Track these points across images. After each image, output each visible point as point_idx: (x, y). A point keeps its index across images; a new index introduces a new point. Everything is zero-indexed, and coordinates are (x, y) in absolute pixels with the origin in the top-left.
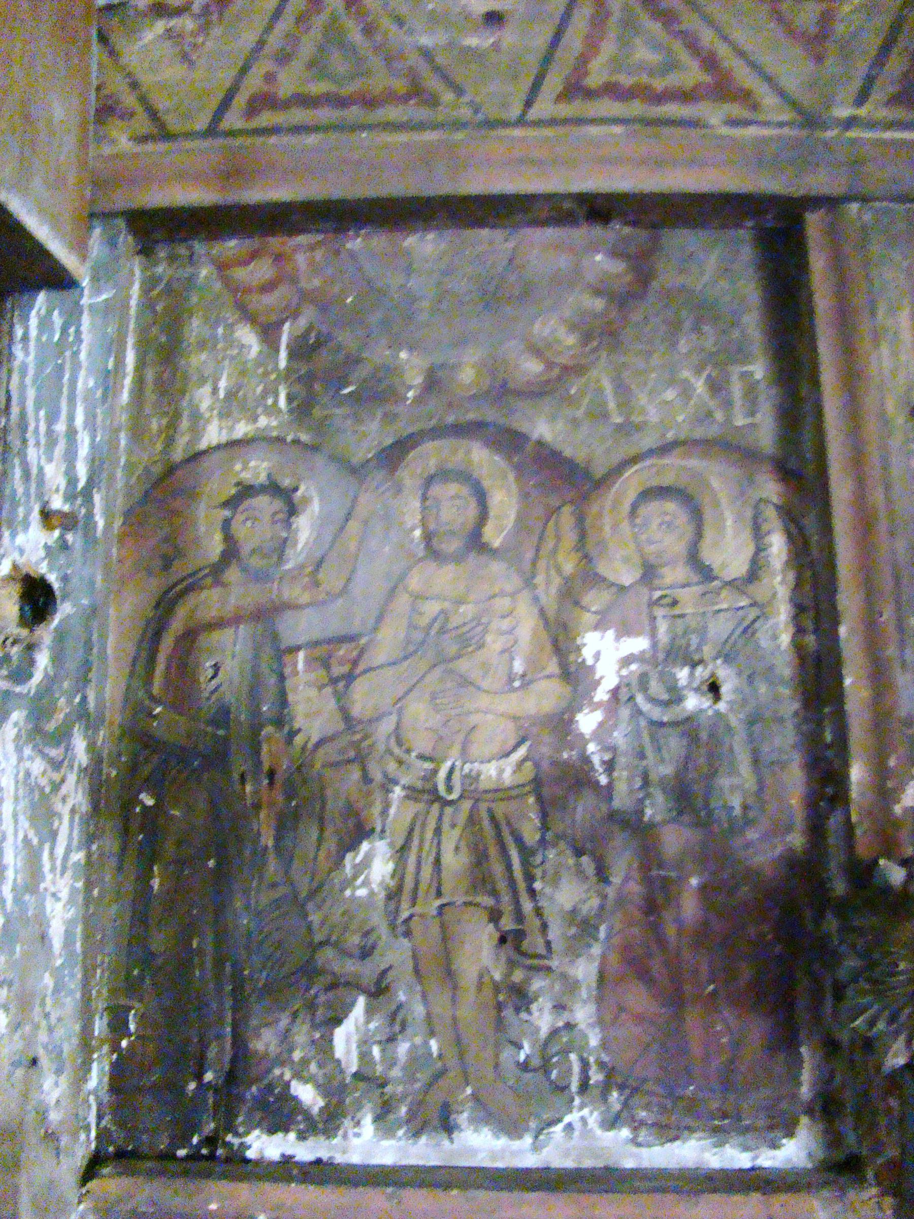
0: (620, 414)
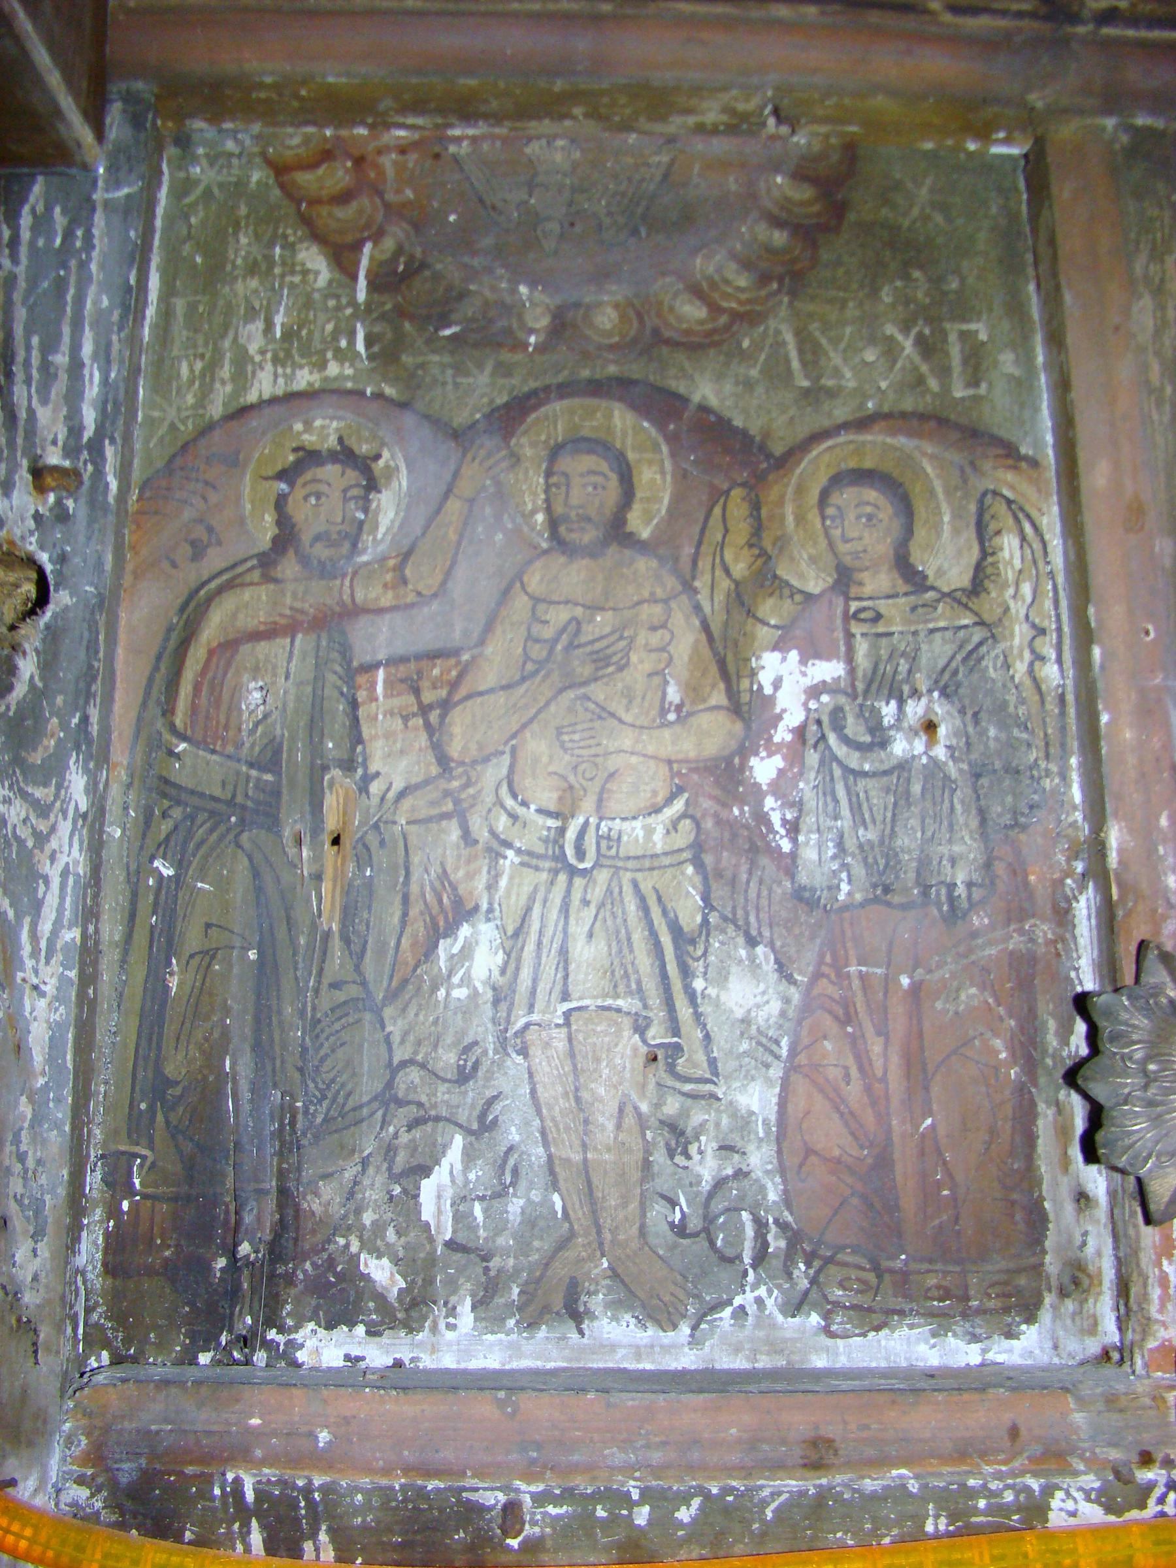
0: (807, 376)
